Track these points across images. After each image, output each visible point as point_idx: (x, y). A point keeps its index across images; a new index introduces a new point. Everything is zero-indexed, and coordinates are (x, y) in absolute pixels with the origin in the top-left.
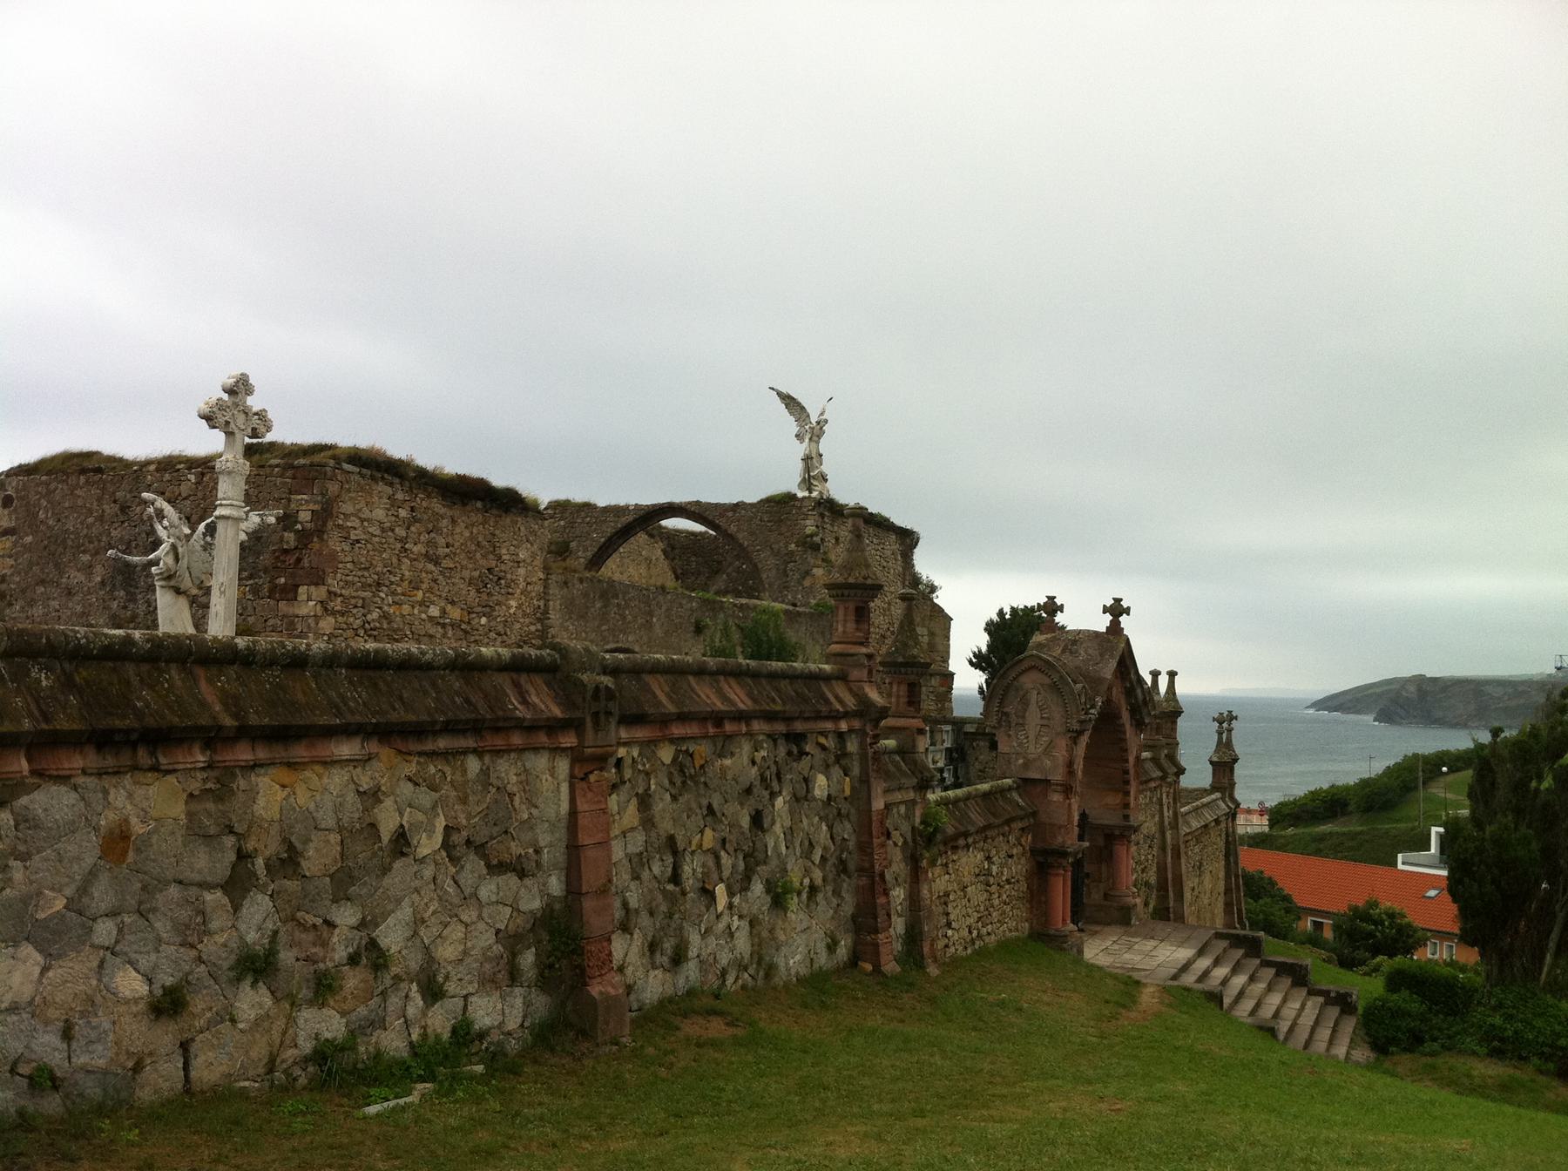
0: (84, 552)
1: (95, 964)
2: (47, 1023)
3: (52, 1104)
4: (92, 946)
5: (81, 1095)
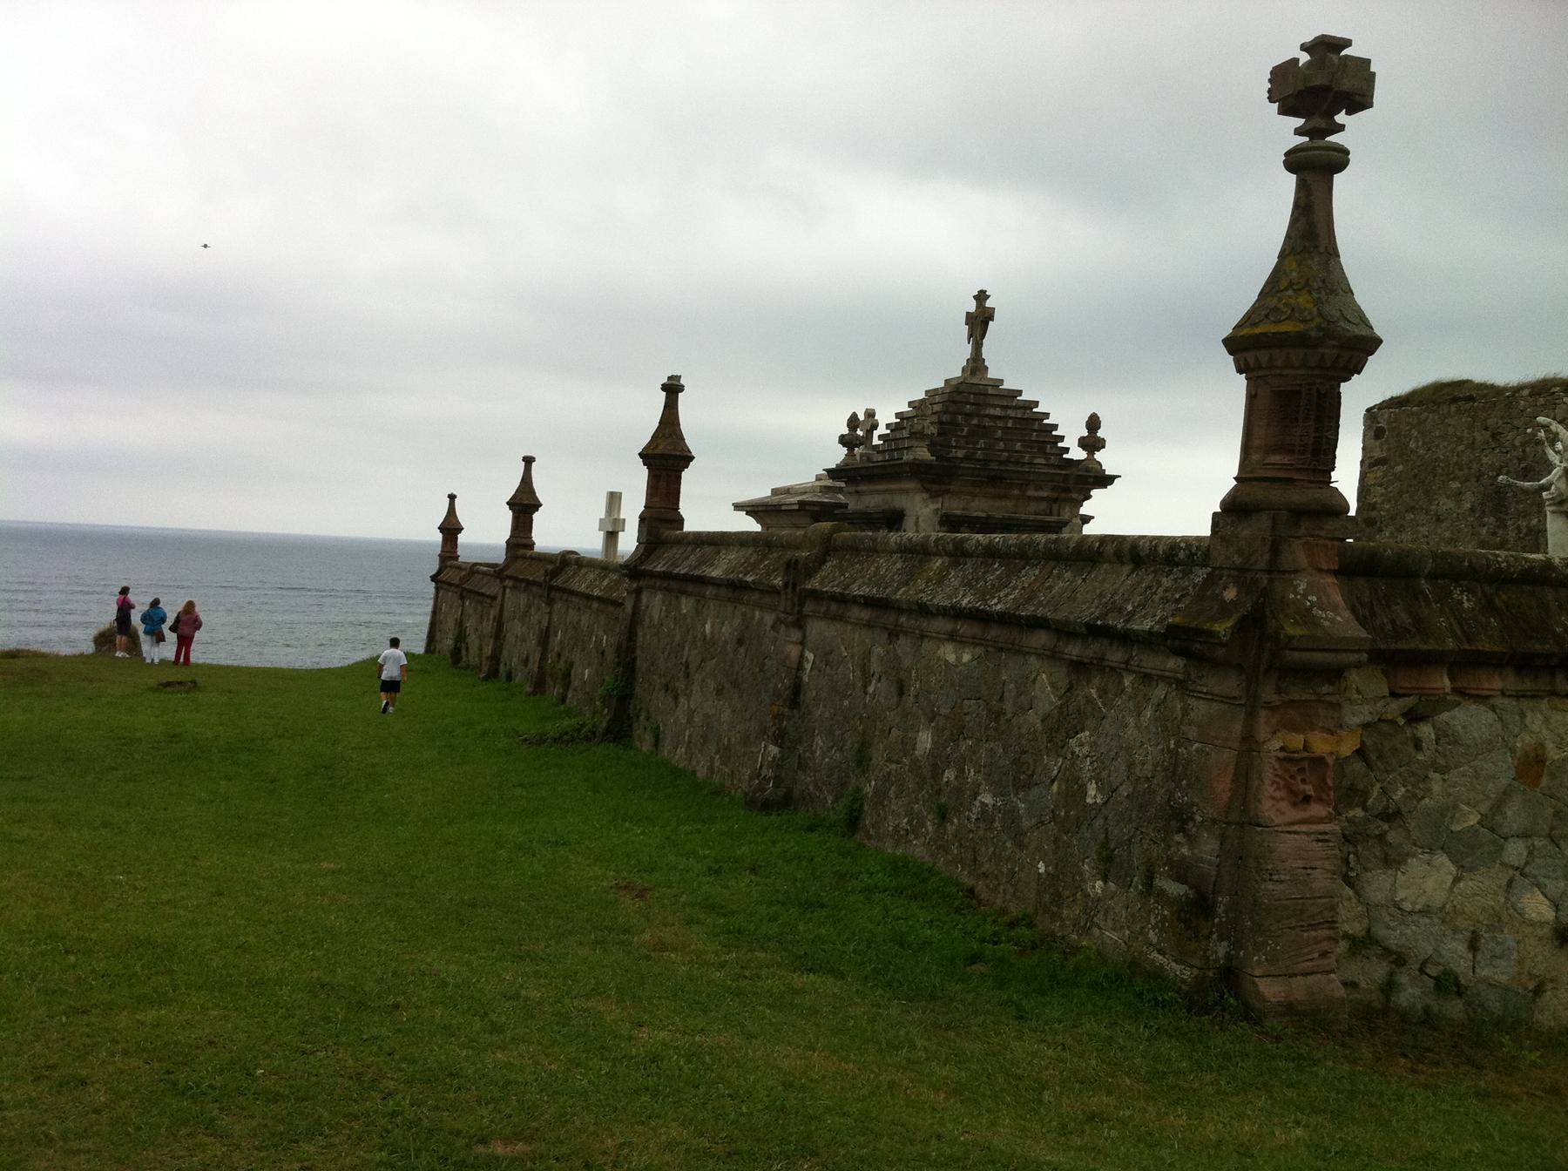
0: (1454, 479)
1: (1504, 882)
2: (1455, 931)
3: (1454, 1009)
4: (1502, 864)
5: (1482, 1006)
